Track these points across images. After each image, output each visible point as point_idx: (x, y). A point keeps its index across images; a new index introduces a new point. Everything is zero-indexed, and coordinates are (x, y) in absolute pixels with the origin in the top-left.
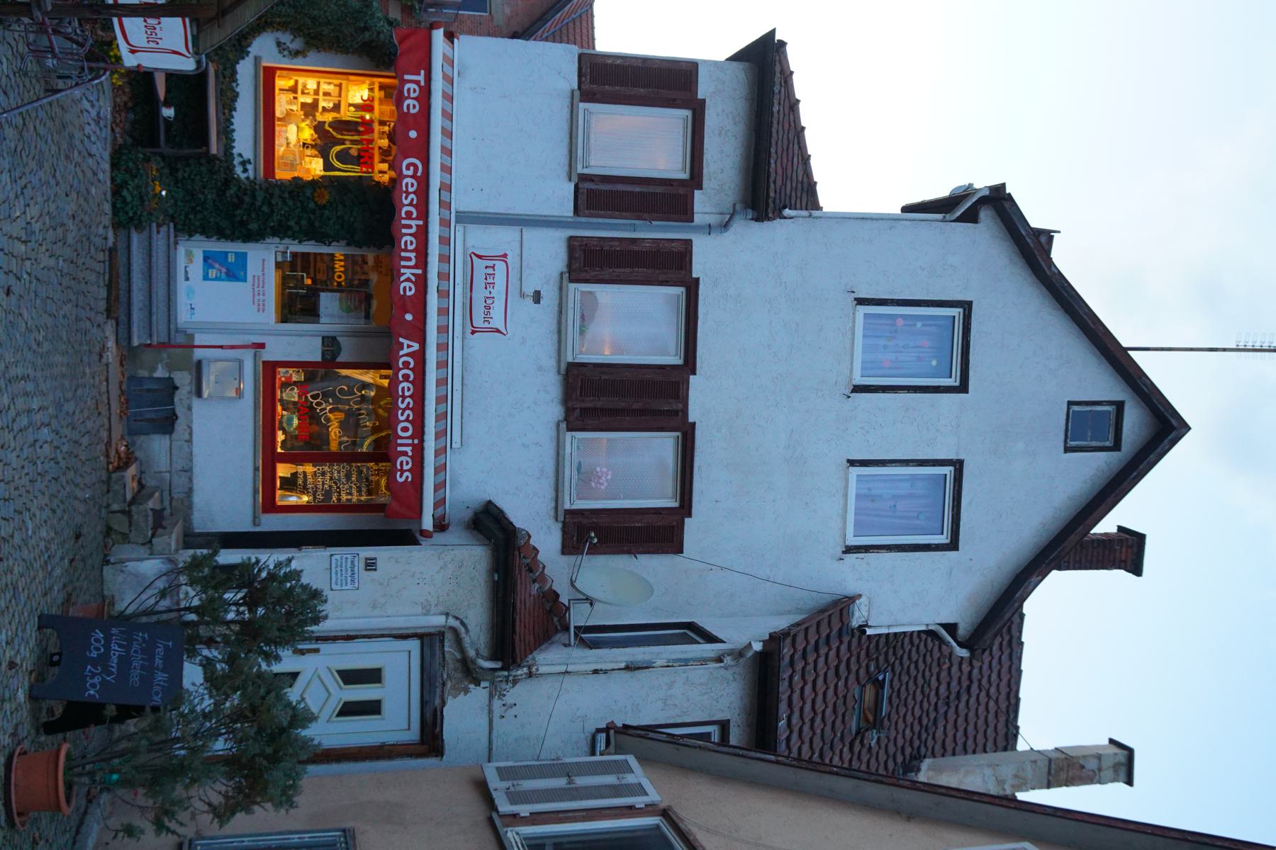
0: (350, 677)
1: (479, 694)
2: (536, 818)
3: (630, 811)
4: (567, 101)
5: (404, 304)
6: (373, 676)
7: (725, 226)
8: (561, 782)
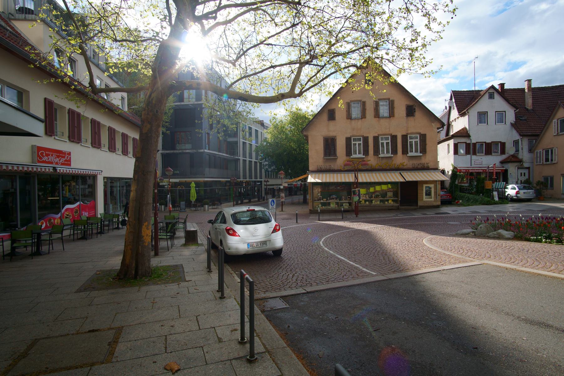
0: (521, 175)
1: (524, 164)
2: (543, 161)
3: (543, 153)
6: (521, 174)
7: (471, 140)
8: (538, 158)
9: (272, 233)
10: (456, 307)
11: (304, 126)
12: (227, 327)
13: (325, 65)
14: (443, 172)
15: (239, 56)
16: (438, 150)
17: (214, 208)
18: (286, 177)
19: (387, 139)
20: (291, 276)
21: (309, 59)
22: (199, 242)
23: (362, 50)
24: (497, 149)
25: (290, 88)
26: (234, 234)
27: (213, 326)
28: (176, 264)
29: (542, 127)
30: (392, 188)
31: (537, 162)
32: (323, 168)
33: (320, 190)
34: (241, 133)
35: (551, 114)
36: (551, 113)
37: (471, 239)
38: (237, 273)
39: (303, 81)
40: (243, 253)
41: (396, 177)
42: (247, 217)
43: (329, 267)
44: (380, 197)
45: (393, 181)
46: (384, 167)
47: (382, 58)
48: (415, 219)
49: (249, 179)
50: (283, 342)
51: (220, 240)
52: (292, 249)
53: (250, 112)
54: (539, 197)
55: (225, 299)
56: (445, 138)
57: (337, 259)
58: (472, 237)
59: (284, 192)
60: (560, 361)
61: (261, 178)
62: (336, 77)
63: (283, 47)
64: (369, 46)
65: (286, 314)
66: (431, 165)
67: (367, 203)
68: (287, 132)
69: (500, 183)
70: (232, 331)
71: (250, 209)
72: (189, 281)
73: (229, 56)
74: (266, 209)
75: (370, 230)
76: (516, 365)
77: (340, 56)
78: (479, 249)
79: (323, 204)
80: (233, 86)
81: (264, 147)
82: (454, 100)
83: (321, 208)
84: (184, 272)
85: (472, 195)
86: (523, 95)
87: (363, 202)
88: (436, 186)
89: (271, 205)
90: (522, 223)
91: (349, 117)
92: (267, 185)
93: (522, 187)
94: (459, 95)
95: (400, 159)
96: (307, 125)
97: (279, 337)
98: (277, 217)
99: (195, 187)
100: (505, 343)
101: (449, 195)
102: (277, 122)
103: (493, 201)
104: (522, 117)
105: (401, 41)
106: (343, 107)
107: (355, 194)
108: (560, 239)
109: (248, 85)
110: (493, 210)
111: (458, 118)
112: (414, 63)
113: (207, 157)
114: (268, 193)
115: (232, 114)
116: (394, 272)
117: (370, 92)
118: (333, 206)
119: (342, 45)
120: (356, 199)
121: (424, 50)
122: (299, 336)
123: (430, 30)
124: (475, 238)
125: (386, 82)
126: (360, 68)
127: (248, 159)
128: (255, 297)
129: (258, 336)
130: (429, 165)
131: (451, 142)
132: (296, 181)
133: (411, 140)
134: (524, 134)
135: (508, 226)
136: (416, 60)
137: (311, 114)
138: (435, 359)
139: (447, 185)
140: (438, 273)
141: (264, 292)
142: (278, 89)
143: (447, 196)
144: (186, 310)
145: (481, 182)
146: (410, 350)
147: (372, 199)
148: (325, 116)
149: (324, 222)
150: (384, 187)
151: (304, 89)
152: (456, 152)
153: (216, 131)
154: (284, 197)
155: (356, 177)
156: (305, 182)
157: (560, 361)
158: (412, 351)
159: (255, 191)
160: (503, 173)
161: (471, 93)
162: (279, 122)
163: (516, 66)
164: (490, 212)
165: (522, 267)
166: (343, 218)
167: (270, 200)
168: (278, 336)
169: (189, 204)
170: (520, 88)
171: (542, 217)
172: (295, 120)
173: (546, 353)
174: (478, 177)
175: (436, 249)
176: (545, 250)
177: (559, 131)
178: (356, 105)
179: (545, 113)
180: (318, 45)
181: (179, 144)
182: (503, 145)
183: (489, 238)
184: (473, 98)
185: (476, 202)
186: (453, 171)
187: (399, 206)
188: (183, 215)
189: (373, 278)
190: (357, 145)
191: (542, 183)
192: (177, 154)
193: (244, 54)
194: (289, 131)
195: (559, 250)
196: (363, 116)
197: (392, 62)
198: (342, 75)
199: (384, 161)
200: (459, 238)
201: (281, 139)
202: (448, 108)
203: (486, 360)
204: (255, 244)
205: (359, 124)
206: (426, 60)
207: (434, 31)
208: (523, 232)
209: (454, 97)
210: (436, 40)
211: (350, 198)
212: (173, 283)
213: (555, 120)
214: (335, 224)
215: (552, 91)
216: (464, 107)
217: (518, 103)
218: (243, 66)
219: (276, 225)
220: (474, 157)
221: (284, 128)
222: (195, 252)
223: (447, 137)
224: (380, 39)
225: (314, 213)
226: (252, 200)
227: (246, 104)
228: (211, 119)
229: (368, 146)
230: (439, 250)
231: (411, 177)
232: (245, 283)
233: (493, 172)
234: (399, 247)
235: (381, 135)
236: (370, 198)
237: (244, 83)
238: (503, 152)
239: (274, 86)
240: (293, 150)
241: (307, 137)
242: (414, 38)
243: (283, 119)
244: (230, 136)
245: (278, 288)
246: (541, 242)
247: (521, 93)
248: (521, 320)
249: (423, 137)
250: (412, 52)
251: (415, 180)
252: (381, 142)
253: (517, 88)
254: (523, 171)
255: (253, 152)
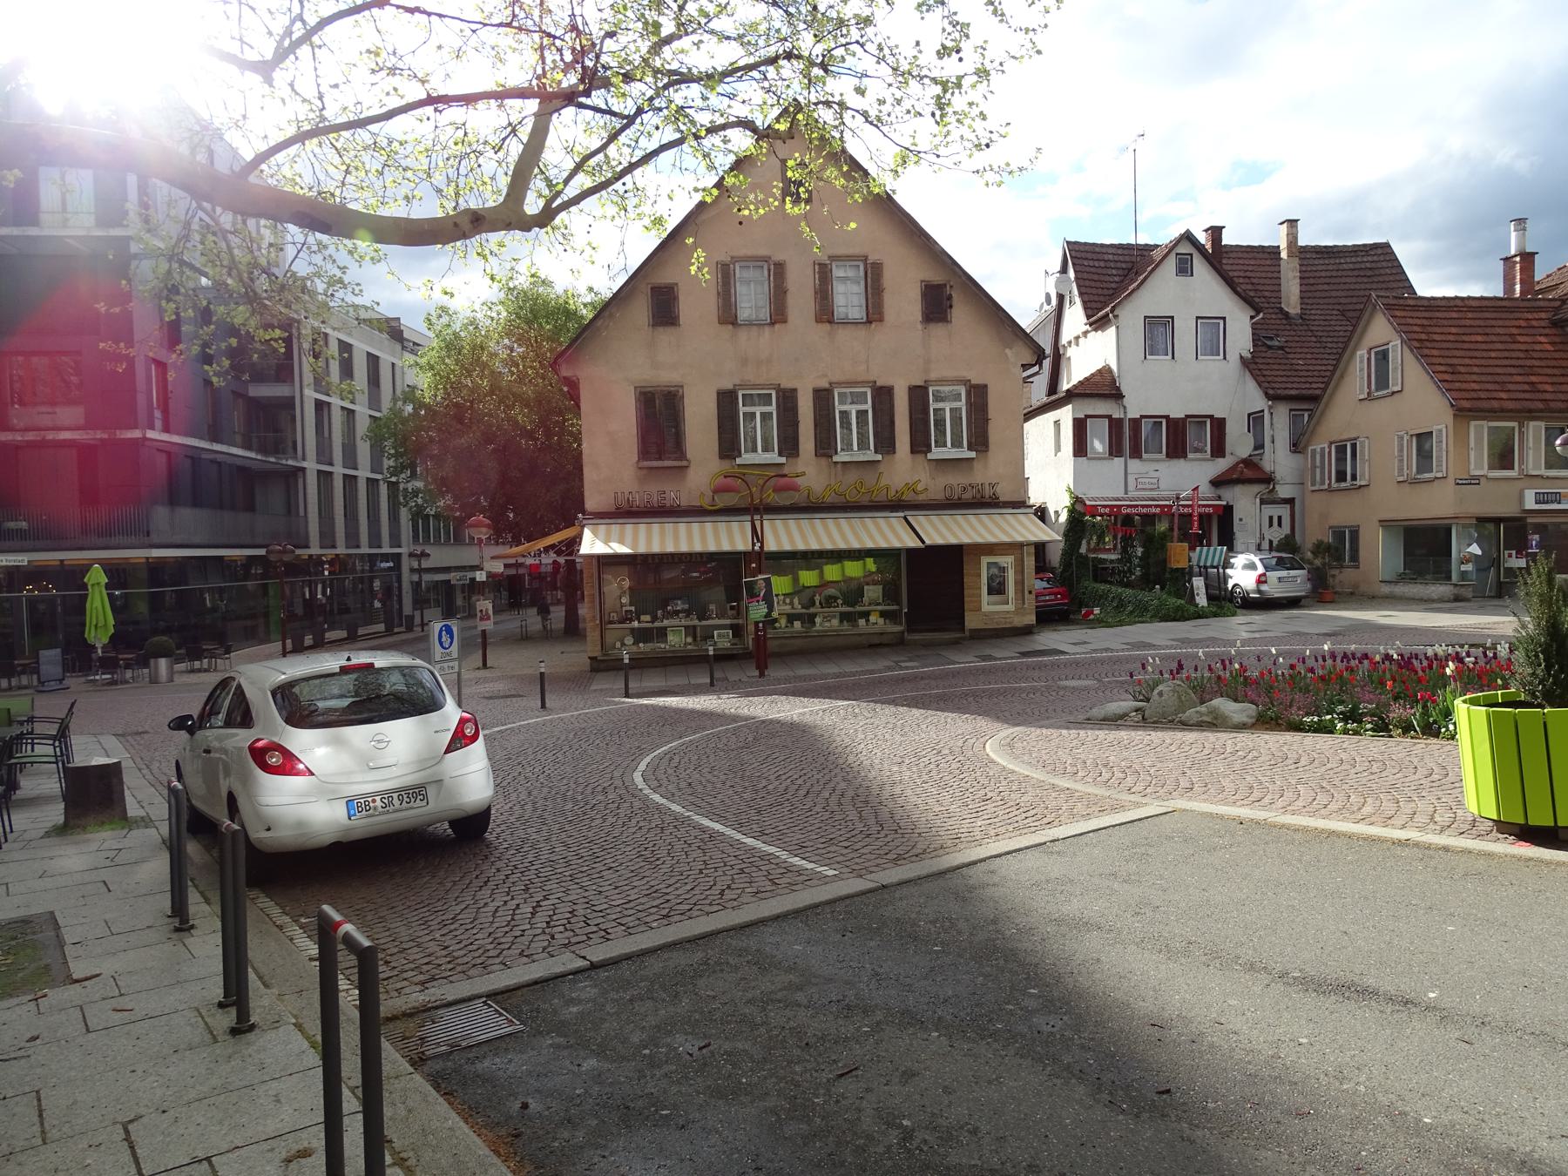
0: (1271, 525)
1: (1277, 487)
2: (1330, 479)
3: (1330, 453)
5: (1162, 512)
6: (1271, 518)
7: (1125, 407)
8: (1318, 471)
9: (448, 751)
10: (1098, 960)
11: (560, 344)
12: (266, 1146)
13: (640, 111)
14: (1041, 513)
15: (287, 43)
16: (1025, 441)
17: (199, 671)
18: (498, 536)
19: (860, 398)
20: (527, 909)
21: (576, 85)
22: (133, 810)
23: (771, 71)
24: (1202, 439)
25: (504, 193)
26: (288, 764)
27: (201, 1155)
28: (22, 913)
29: (1328, 374)
30: (879, 571)
31: (1313, 484)
32: (638, 501)
33: (627, 584)
34: (307, 362)
35: (1352, 331)
36: (1350, 328)
37: (1133, 733)
38: (303, 920)
39: (556, 171)
40: (328, 839)
41: (890, 533)
42: (342, 696)
43: (669, 862)
44: (840, 601)
45: (884, 545)
46: (852, 497)
47: (842, 104)
48: (955, 674)
49: (347, 547)
50: (504, 1169)
51: (224, 794)
52: (529, 807)
53: (341, 281)
54: (1322, 592)
55: (257, 1031)
56: (1045, 399)
57: (696, 832)
58: (1135, 727)
59: (492, 595)
60: (1403, 1100)
61: (395, 540)
62: (678, 164)
63: (474, 26)
64: (799, 57)
65: (510, 1061)
66: (1005, 493)
67: (797, 624)
68: (498, 366)
69: (1212, 548)
70: (288, 1161)
71: (354, 661)
72: (87, 979)
73: (241, 40)
74: (418, 662)
75: (808, 719)
76: (1284, 1132)
77: (694, 86)
78: (1159, 765)
79: (642, 635)
80: (264, 166)
81: (404, 421)
82: (1071, 274)
83: (634, 649)
84: (61, 944)
85: (1129, 591)
86: (1273, 269)
87: (783, 622)
88: (1022, 560)
89: (441, 643)
90: (1277, 675)
91: (728, 316)
92: (420, 571)
93: (1274, 561)
94: (1089, 256)
95: (903, 470)
96: (574, 341)
97: (487, 1151)
98: (465, 691)
99: (107, 586)
100: (1249, 1062)
101: (1061, 590)
102: (457, 327)
103: (1192, 609)
104: (1271, 339)
105: (907, 50)
106: (708, 277)
107: (753, 595)
108: (1381, 718)
109: (331, 169)
110: (1193, 636)
111: (1085, 333)
112: (948, 133)
113: (161, 460)
114: (428, 601)
115: (262, 283)
116: (896, 861)
117: (803, 224)
118: (676, 640)
119: (701, 41)
120: (758, 611)
121: (982, 87)
122: (566, 1135)
123: (1001, 21)
124: (1144, 728)
125: (857, 191)
126: (762, 134)
127: (339, 470)
128: (382, 1008)
129: (400, 1162)
130: (998, 490)
131: (1066, 415)
132: (536, 553)
133: (940, 405)
134: (1279, 392)
135: (1237, 683)
136: (958, 121)
137: (588, 300)
138: (1045, 1147)
139: (1055, 556)
140: (1035, 853)
141: (422, 983)
142: (457, 194)
143: (1056, 594)
144: (75, 1103)
145: (1157, 545)
146: (962, 1128)
147: (812, 610)
148: (641, 310)
149: (645, 701)
150: (853, 569)
151: (558, 201)
152: (1080, 449)
153: (196, 349)
154: (491, 612)
155: (757, 535)
156: (571, 554)
157: (1403, 1100)
158: (968, 1131)
159: (373, 594)
160: (1219, 516)
161: (1126, 252)
162: (465, 326)
163: (1254, 174)
164: (1185, 642)
165: (1283, 813)
166: (712, 684)
167: (437, 626)
168: (483, 1150)
169: (80, 658)
170: (1266, 244)
171: (1333, 656)
172: (529, 322)
173: (1363, 1078)
174: (1148, 529)
175: (1027, 773)
176: (1344, 756)
177: (1373, 387)
178: (751, 274)
179: (1336, 328)
180: (611, 35)
181: (22, 403)
182: (1219, 425)
183: (1185, 725)
184: (1130, 270)
185: (1142, 613)
186: (1072, 511)
187: (903, 632)
188: (51, 706)
189: (828, 887)
190: (758, 420)
191: (1328, 548)
192: (17, 447)
193: (307, 37)
194: (503, 361)
195: (1382, 753)
196: (779, 316)
197: (876, 123)
198: (701, 158)
199: (852, 477)
200: (1097, 732)
201: (472, 391)
202: (1054, 302)
203: (1197, 1126)
204: (378, 798)
205: (762, 342)
206: (989, 125)
207: (1014, 23)
208: (1281, 704)
209: (1074, 264)
210: (1022, 57)
211: (738, 610)
212: (11, 996)
213: (1362, 353)
214: (685, 705)
215: (1353, 260)
216: (1102, 299)
217: (1259, 294)
218: (308, 89)
219: (462, 721)
220: (1134, 465)
221: (482, 348)
222: (111, 854)
223: (1053, 398)
224: (835, 37)
225: (607, 670)
226: (361, 631)
227: (325, 247)
228: (169, 300)
229: (795, 424)
230: (1038, 775)
231: (941, 531)
232: (340, 959)
233: (1191, 515)
234: (908, 773)
235: (840, 384)
236: (807, 608)
237: (313, 160)
238: (1219, 450)
239: (439, 179)
240: (521, 436)
241: (573, 390)
242: (949, 44)
243: (479, 316)
244: (259, 377)
245: (479, 961)
246: (1331, 732)
247: (1268, 262)
248: (1291, 981)
249: (978, 395)
250: (945, 91)
251: (953, 541)
252: (838, 407)
253: (1245, 244)
254: (1271, 510)
255: (359, 443)
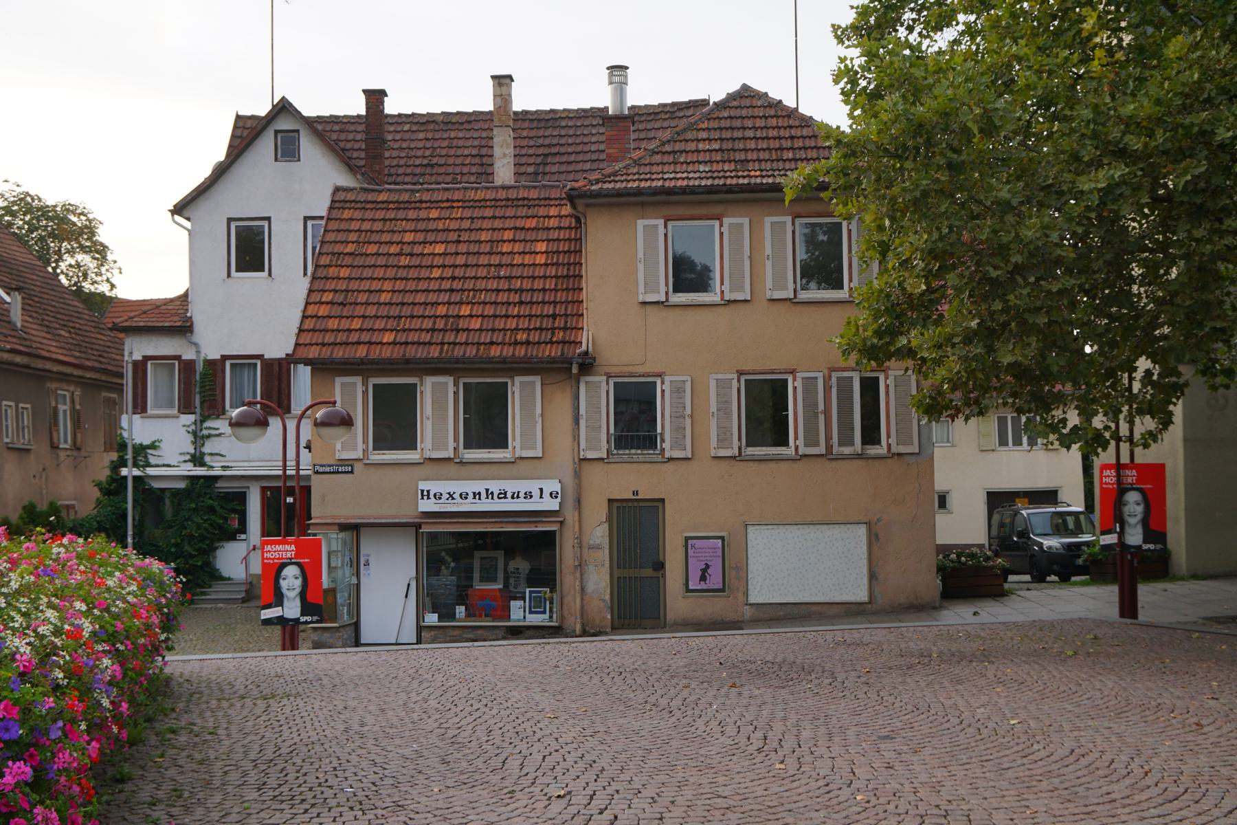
2: (828, 438)
4: (146, 420)
7: (196, 344)
